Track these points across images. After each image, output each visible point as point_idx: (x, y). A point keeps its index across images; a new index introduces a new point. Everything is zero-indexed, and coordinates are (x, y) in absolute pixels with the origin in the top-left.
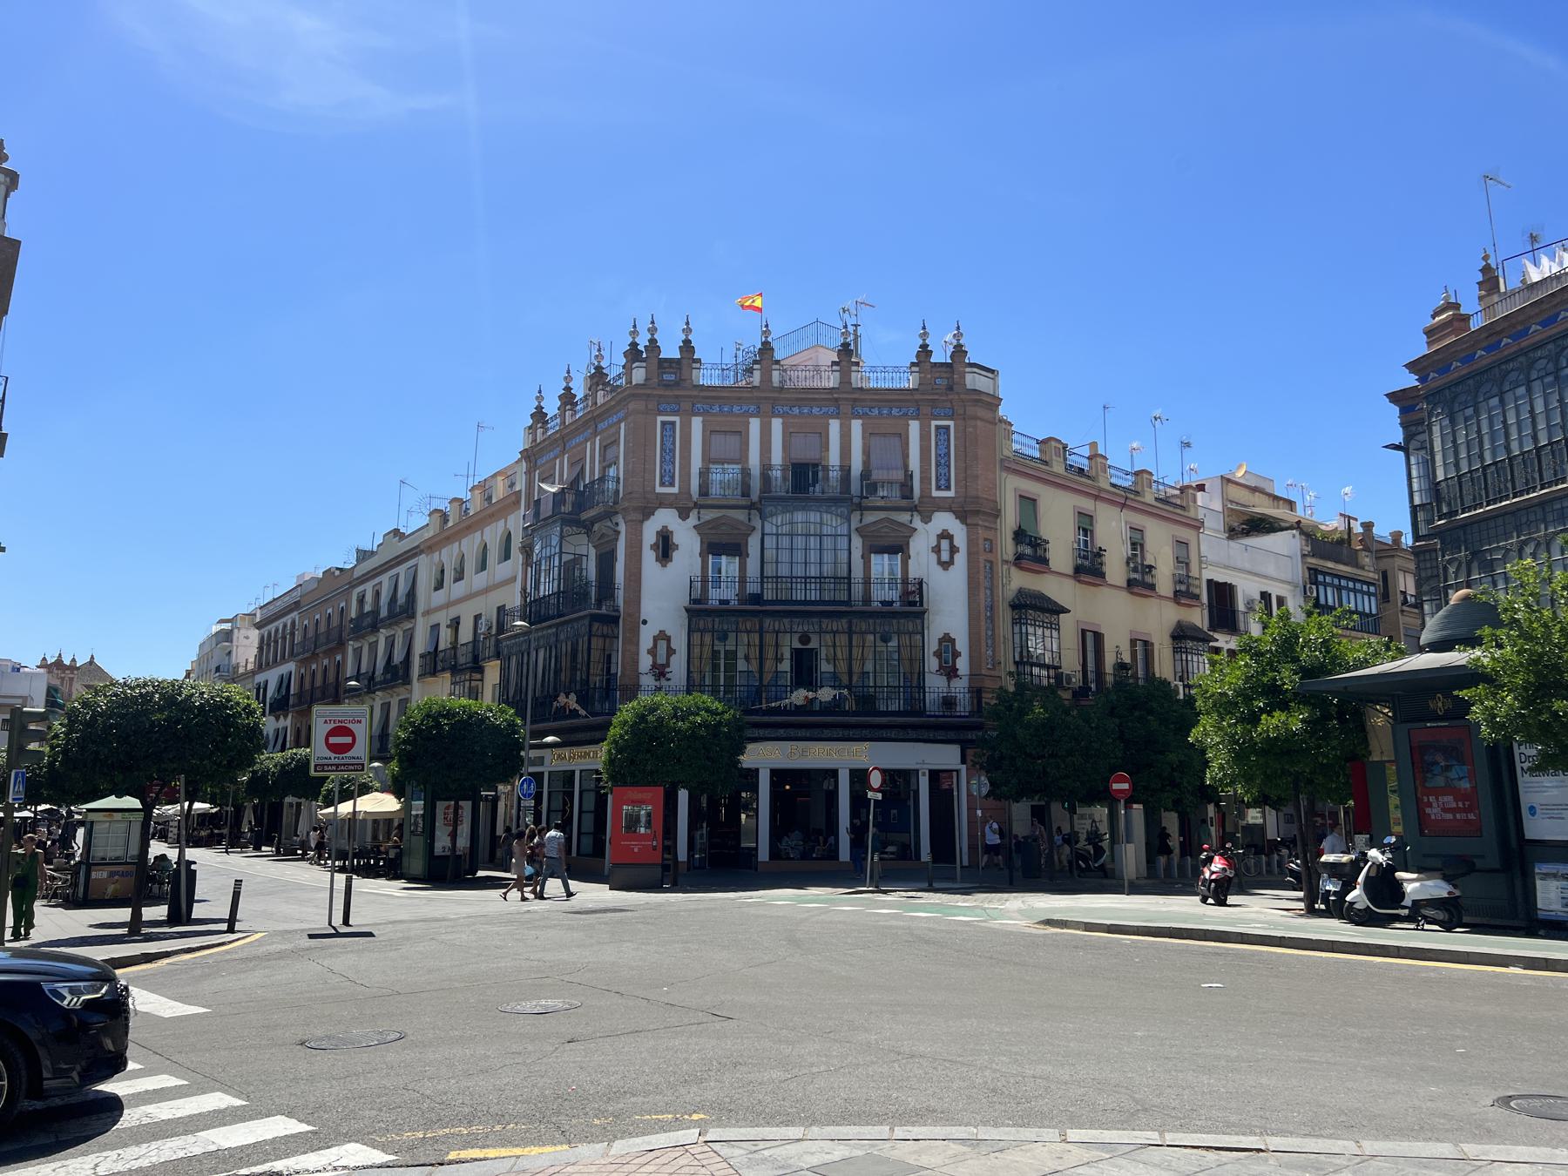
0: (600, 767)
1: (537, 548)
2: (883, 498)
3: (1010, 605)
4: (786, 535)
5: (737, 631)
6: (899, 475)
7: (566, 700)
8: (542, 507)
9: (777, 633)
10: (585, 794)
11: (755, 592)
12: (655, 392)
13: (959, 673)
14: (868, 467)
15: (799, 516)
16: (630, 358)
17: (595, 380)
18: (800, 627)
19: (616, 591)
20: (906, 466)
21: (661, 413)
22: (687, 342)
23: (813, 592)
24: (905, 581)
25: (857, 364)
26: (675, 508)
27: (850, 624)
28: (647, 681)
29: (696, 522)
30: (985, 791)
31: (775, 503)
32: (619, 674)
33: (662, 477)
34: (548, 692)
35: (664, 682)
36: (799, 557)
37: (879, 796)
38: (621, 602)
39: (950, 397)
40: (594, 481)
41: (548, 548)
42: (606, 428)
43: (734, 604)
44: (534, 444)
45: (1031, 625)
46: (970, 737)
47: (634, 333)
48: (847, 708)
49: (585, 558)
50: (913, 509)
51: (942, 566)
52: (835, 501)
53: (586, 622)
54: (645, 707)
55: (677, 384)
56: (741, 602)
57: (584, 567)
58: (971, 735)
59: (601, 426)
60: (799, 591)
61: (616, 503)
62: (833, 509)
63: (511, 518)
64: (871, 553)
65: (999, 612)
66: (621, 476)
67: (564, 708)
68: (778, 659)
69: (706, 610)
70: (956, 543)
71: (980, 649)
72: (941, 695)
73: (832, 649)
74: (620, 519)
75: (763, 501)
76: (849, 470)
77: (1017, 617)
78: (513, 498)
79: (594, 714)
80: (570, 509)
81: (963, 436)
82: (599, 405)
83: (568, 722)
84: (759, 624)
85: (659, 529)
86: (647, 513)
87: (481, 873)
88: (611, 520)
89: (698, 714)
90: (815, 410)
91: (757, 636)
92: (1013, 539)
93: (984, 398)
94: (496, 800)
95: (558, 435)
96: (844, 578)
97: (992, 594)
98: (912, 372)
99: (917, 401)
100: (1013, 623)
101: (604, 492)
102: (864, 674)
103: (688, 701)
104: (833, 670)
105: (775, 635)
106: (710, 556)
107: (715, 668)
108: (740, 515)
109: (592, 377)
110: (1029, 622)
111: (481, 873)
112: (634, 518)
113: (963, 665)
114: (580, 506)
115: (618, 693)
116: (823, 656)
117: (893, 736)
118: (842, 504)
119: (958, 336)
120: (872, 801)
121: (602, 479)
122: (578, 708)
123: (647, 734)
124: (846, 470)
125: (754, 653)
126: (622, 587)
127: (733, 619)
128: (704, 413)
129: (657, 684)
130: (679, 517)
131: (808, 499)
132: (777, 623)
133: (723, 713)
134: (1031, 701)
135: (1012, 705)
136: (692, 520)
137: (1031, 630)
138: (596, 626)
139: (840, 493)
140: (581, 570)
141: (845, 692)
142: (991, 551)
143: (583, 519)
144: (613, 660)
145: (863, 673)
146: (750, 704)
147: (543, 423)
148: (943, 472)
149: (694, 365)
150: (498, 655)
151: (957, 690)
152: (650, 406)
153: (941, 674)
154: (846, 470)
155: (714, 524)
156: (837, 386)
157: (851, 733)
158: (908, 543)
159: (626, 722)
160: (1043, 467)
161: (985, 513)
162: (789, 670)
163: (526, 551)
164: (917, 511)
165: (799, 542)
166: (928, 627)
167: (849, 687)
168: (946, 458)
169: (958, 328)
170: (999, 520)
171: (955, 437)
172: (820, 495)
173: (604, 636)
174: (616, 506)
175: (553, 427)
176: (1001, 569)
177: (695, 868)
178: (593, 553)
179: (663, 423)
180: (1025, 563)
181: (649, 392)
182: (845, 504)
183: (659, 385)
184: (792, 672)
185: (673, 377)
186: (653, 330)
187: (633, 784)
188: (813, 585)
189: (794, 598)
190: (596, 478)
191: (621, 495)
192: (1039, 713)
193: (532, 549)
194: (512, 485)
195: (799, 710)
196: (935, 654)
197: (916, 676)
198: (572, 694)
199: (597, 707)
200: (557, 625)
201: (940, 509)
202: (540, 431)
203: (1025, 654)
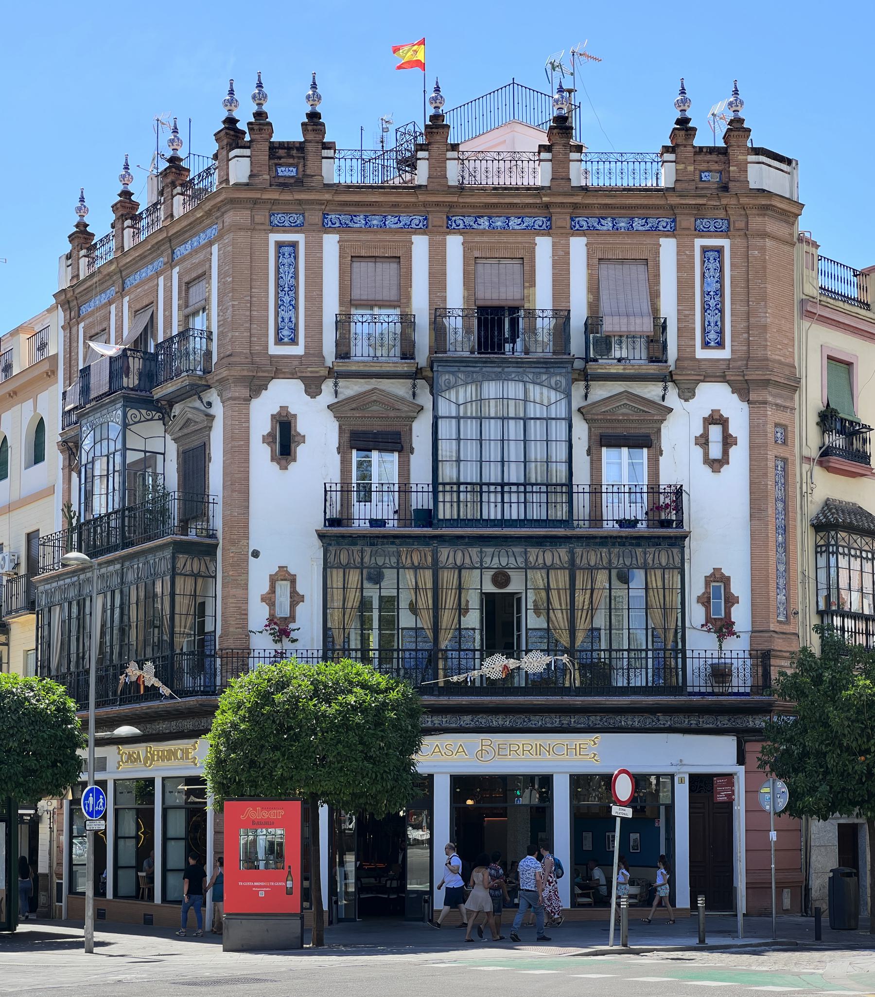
0: (203, 773)
1: (87, 444)
2: (619, 360)
3: (813, 525)
4: (472, 418)
5: (398, 567)
6: (646, 326)
7: (138, 673)
8: (93, 380)
9: (460, 569)
10: (171, 814)
11: (425, 507)
12: (266, 196)
13: (736, 628)
14: (598, 312)
15: (491, 389)
16: (225, 142)
17: (169, 180)
18: (496, 560)
19: (211, 505)
20: (655, 310)
21: (275, 228)
22: (314, 116)
23: (514, 506)
24: (654, 489)
25: (579, 149)
26: (299, 378)
27: (572, 554)
28: (262, 643)
29: (332, 400)
30: (782, 802)
31: (456, 369)
32: (218, 633)
33: (278, 330)
34: (111, 660)
35: (286, 644)
36: (492, 452)
37: (628, 813)
38: (218, 523)
39: (724, 201)
40: (172, 338)
41: (105, 443)
42: (190, 254)
43: (392, 526)
44: (75, 282)
45: (844, 554)
46: (751, 724)
47: (231, 101)
48: (567, 684)
49: (160, 458)
50: (667, 378)
51: (711, 466)
52: (545, 365)
53: (168, 553)
54: (269, 680)
55: (299, 183)
56: (403, 521)
57: (159, 470)
58: (759, 722)
59: (182, 251)
60: (492, 505)
61: (207, 371)
62: (544, 377)
63: (43, 397)
64: (602, 446)
65: (795, 536)
66: (215, 329)
67: (136, 684)
68: (461, 610)
69: (384, 537)
70: (732, 431)
71: (768, 593)
72: (709, 662)
73: (543, 594)
74: (213, 396)
75: (435, 365)
76: (568, 318)
77: (822, 543)
78: (46, 367)
79: (183, 693)
80: (137, 382)
81: (744, 258)
82: (176, 217)
83: (143, 705)
84: (433, 559)
85: (276, 410)
86: (257, 386)
87: (22, 928)
88: (200, 398)
89: (350, 692)
90: (514, 222)
91: (428, 574)
92: (818, 424)
93: (777, 203)
94: (35, 822)
95: (113, 267)
96: (562, 485)
97: (785, 509)
98: (540, 160)
99: (672, 207)
100: (817, 552)
101: (188, 354)
102: (594, 631)
103: (334, 671)
104: (545, 626)
105: (457, 572)
106: (354, 452)
107: (365, 624)
108: (399, 388)
109: (165, 174)
110: (841, 550)
111: (22, 928)
112: (237, 394)
113: (741, 616)
114: (149, 378)
115: (218, 661)
116: (530, 605)
117: (636, 724)
118: (557, 370)
119: (736, 104)
120: (618, 820)
121: (184, 335)
122: (158, 684)
123: (274, 722)
124: (562, 316)
125: (425, 601)
126: (219, 499)
127: (392, 549)
128: (342, 229)
129: (278, 647)
130: (306, 392)
131: (505, 361)
132: (459, 555)
133: (387, 690)
134: (849, 669)
135: (821, 676)
136: (327, 395)
137: (843, 562)
138: (182, 559)
139: (554, 353)
140: (155, 475)
141: (565, 658)
142: (785, 443)
143: (156, 397)
144: (209, 611)
145: (592, 630)
146: (420, 677)
147: (88, 249)
148: (287, 316)
149: (325, 153)
150: (31, 606)
151: (734, 655)
152: (259, 218)
153: (709, 631)
154: (562, 316)
155: (358, 402)
156: (547, 184)
157: (573, 720)
158: (659, 430)
159: (239, 705)
160: (863, 312)
161: (777, 384)
162: (477, 626)
163: (69, 449)
164: (673, 381)
165: (492, 429)
166: (690, 559)
167: (570, 651)
168: (717, 298)
169: (736, 92)
170: (797, 396)
171: (732, 265)
172: (523, 356)
173: (196, 576)
174: (208, 376)
175: (105, 254)
176: (799, 470)
177: (340, 920)
178: (172, 449)
179: (280, 245)
180: (835, 461)
181: (257, 195)
182: (564, 370)
183: (271, 185)
184: (482, 630)
185: (292, 172)
186: (260, 97)
187: (255, 797)
188: (492, 496)
189: (485, 517)
190: (175, 332)
191: (215, 359)
192: (866, 687)
193: (78, 446)
194: (42, 347)
195: (491, 686)
196: (699, 600)
197: (672, 632)
198: (149, 664)
199: (188, 681)
200: (123, 559)
201: (707, 378)
202: (83, 262)
203: (833, 599)
